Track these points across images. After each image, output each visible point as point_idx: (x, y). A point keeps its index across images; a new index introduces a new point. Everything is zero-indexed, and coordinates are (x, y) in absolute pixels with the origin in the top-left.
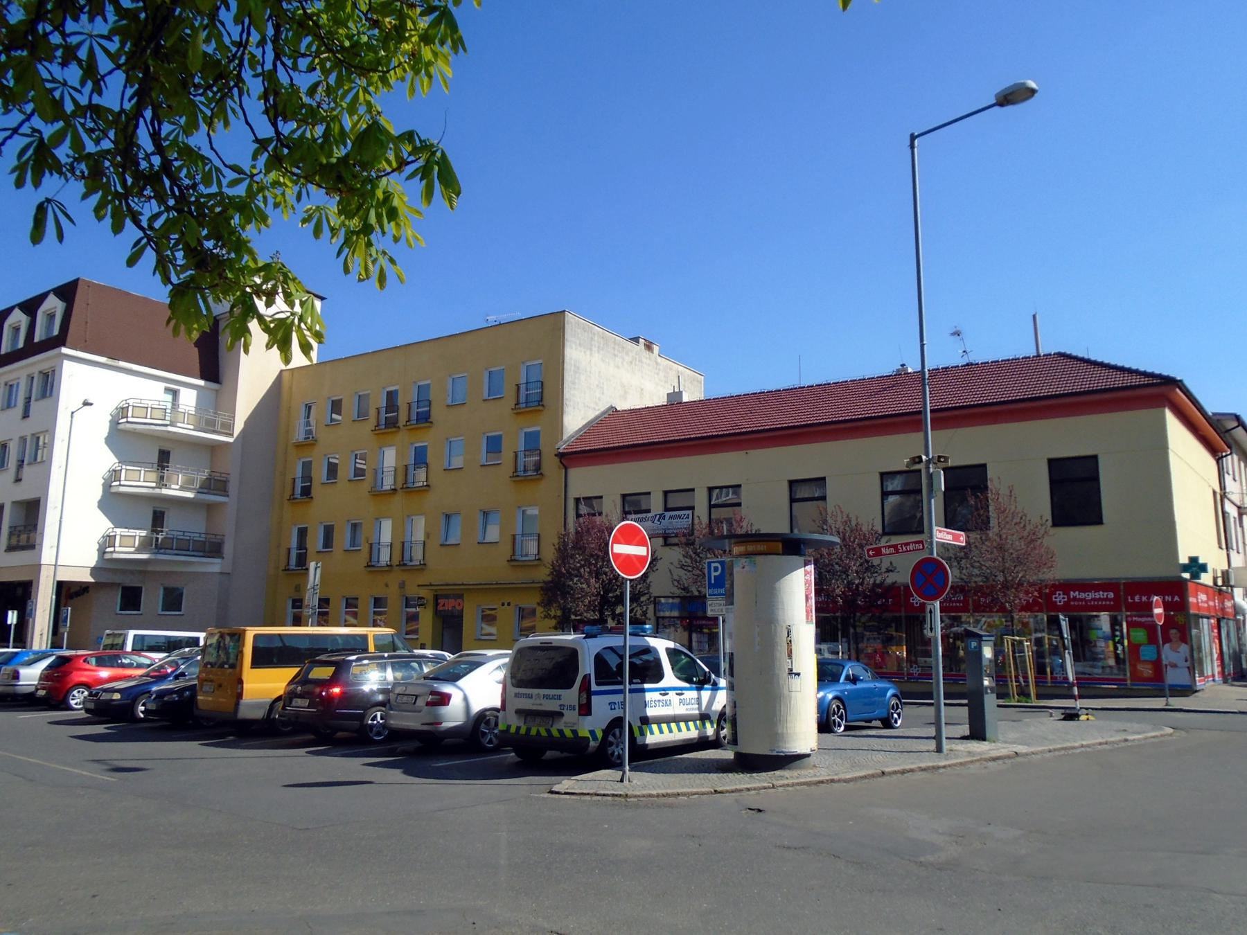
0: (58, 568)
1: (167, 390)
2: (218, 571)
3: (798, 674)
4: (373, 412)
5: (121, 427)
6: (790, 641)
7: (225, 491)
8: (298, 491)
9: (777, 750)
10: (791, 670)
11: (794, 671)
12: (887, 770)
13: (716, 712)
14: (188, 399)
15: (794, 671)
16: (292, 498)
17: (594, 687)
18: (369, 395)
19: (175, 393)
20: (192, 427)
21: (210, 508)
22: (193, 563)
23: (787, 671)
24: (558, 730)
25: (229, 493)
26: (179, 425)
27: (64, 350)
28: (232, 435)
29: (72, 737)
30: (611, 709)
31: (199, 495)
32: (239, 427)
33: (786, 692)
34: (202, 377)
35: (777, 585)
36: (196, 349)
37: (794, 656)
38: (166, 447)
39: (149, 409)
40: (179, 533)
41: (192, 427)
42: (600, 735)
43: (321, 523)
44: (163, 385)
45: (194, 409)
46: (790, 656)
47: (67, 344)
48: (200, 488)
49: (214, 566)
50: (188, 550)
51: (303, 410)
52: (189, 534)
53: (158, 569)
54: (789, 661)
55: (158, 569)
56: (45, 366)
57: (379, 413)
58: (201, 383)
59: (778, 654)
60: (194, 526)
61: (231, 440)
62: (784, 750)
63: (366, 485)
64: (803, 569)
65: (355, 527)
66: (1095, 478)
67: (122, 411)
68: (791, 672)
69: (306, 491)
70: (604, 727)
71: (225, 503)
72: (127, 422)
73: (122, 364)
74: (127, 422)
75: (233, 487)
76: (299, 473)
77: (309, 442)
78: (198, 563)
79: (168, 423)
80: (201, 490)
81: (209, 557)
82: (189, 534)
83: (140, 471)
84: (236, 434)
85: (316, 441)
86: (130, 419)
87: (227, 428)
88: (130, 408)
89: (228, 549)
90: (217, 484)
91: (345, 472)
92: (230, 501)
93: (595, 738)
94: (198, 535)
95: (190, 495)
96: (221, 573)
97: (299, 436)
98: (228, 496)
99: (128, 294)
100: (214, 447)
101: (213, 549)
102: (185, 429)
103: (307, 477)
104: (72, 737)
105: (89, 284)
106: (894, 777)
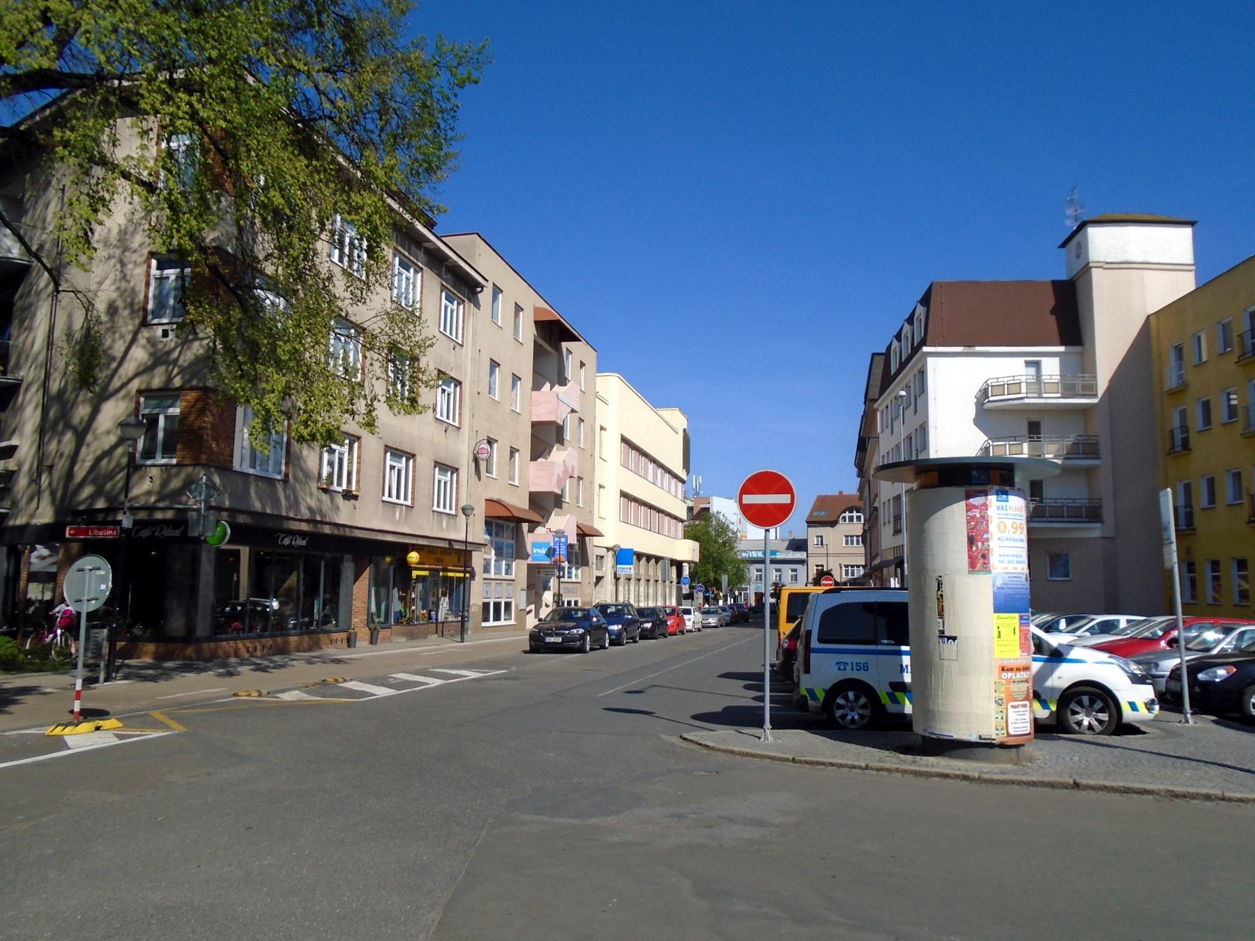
0: (470, 540)
1: (1028, 364)
2: (1100, 535)
3: (954, 638)
4: (1236, 341)
5: (985, 407)
6: (942, 596)
7: (1097, 454)
8: (1178, 443)
9: (930, 730)
10: (943, 632)
11: (947, 634)
12: (1084, 781)
13: (1053, 689)
14: (1051, 368)
15: (947, 634)
16: (1172, 452)
17: (815, 644)
18: (1230, 322)
19: (1037, 365)
20: (1059, 395)
21: (1089, 472)
22: (1079, 529)
23: (937, 634)
24: (806, 689)
25: (1101, 456)
26: (1045, 395)
27: (925, 349)
28: (1095, 396)
29: (723, 676)
30: (839, 669)
31: (1067, 461)
32: (1102, 384)
33: (936, 659)
34: (1062, 344)
35: (926, 526)
36: (1053, 318)
37: (946, 614)
38: (1035, 418)
39: (1006, 386)
40: (1069, 501)
41: (1059, 395)
42: (821, 695)
43: (1203, 476)
44: (1022, 360)
45: (1059, 377)
46: (941, 614)
47: (928, 343)
48: (1067, 454)
49: (1095, 531)
50: (1063, 517)
51: (1172, 355)
52: (1063, 501)
53: (1047, 537)
54: (941, 620)
55: (1043, 537)
56: (919, 366)
57: (1242, 340)
58: (1062, 349)
59: (928, 613)
60: (1075, 493)
61: (1095, 401)
62: (936, 732)
63: (1239, 428)
64: (962, 504)
65: (1237, 476)
66: (598, 364)
67: (984, 393)
68: (942, 634)
69: (1186, 444)
70: (828, 686)
71: (1097, 467)
72: (989, 401)
73: (978, 349)
74: (989, 401)
75: (1104, 449)
76: (1176, 423)
77: (1180, 390)
78: (1085, 529)
79: (1025, 395)
80: (1069, 456)
81: (1089, 522)
82: (1063, 501)
83: (1005, 445)
84: (1100, 393)
85: (1187, 385)
86: (991, 399)
87: (1090, 390)
88: (990, 388)
89: (1108, 513)
90: (1086, 448)
91: (1220, 414)
92: (1104, 464)
93: (814, 697)
94: (1053, 501)
95: (1059, 462)
96: (1103, 537)
97: (1171, 382)
98: (1099, 458)
99: (978, 283)
100: (1084, 411)
101: (1093, 514)
102: (1053, 398)
103: (1184, 428)
104: (723, 676)
105: (941, 285)
106: (830, 768)
